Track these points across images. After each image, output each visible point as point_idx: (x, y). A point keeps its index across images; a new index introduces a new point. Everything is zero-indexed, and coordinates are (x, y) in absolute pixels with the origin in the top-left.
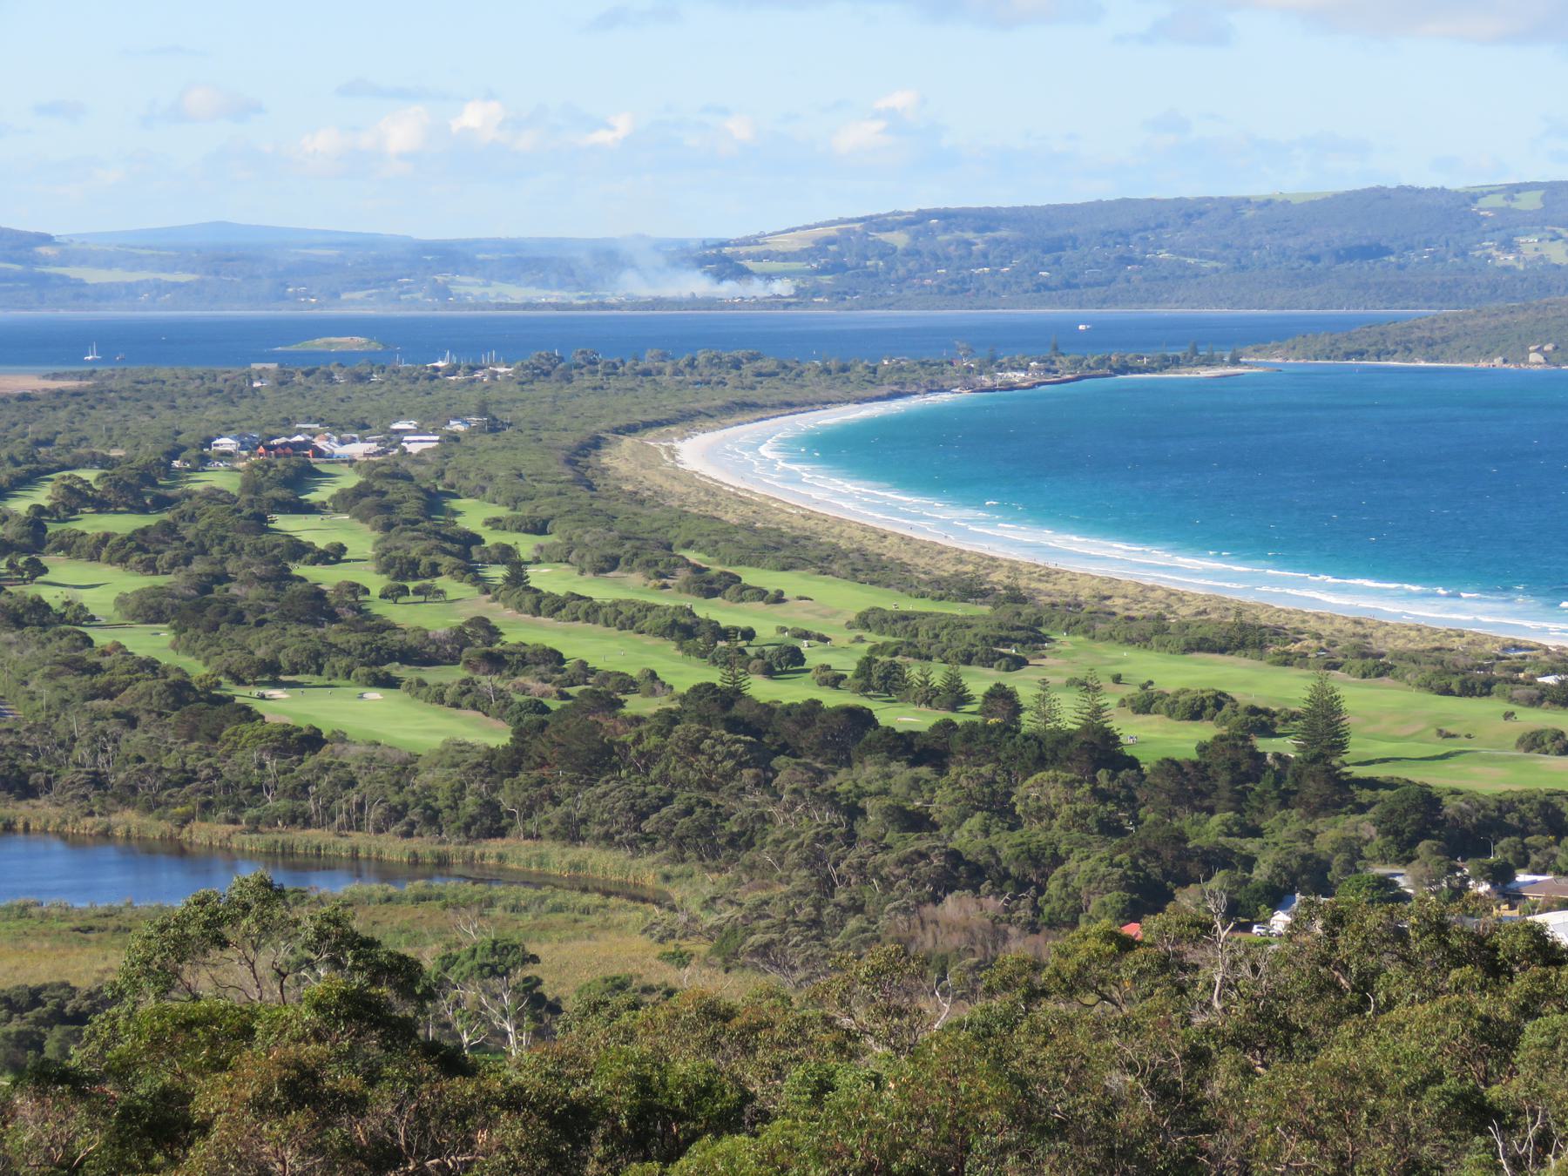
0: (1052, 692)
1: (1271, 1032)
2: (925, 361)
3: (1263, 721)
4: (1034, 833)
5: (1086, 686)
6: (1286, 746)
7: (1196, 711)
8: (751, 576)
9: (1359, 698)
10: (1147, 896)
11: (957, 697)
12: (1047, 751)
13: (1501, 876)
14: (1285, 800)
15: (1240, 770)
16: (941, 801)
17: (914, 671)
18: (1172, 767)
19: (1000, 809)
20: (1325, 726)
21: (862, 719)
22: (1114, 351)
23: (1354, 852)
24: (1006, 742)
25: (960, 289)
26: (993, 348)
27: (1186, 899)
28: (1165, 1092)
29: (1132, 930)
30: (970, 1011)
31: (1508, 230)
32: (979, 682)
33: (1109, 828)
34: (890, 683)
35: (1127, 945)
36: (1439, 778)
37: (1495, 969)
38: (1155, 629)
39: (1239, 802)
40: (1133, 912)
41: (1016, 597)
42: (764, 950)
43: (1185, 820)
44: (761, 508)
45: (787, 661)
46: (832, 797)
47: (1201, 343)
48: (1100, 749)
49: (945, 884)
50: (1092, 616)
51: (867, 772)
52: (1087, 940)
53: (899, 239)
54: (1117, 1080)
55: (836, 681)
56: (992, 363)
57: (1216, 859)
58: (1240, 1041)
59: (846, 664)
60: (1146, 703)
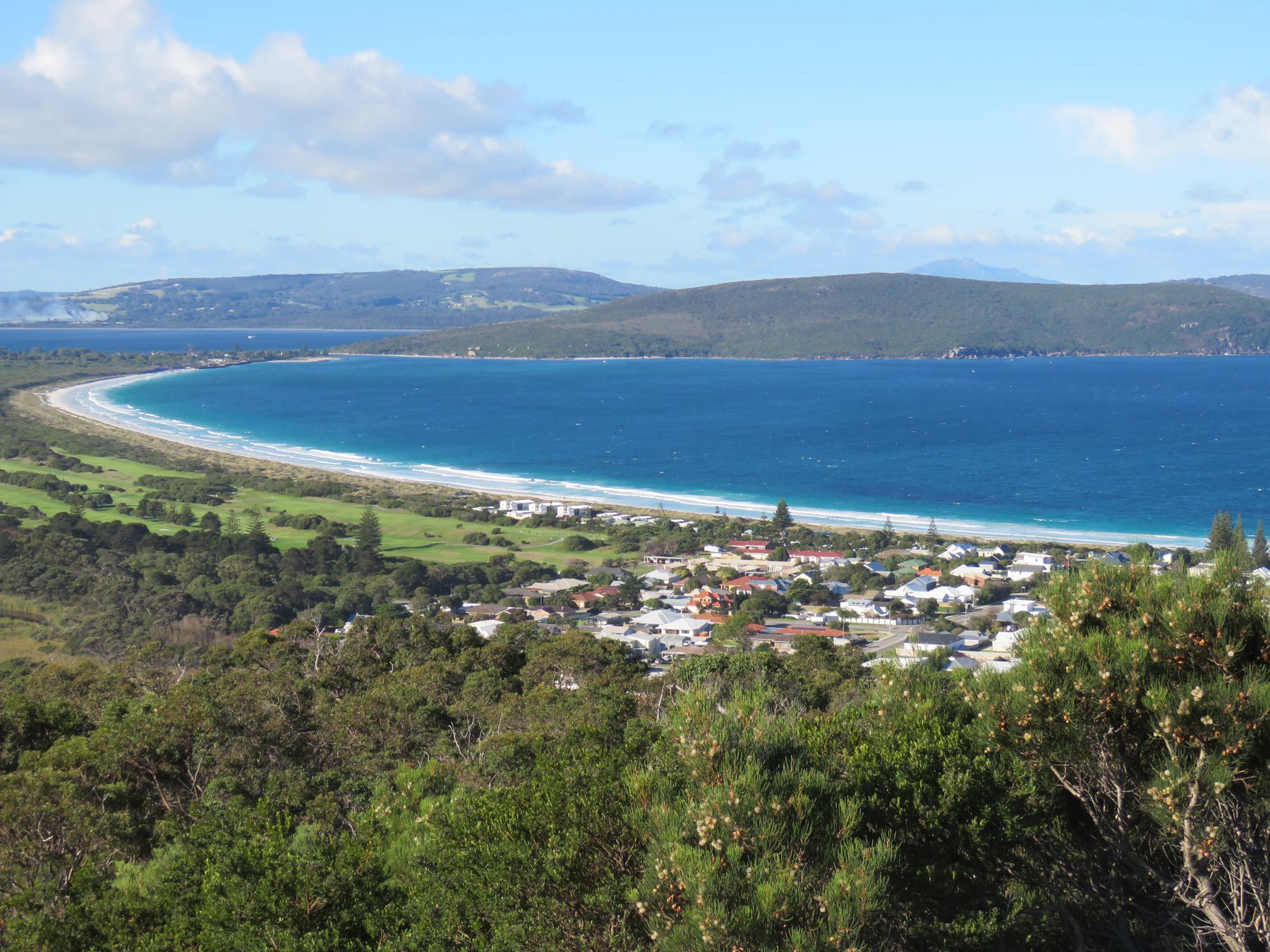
0: (236, 516)
1: (343, 681)
2: (172, 353)
3: (341, 529)
4: (228, 585)
6: (352, 542)
8: (86, 460)
9: (387, 518)
10: (283, 615)
11: (189, 519)
12: (234, 545)
13: (456, 604)
14: (351, 568)
15: (327, 554)
16: (181, 569)
17: (167, 506)
18: (295, 552)
20: (370, 531)
21: (142, 530)
22: (267, 348)
23: (384, 594)
24: (213, 541)
25: (190, 318)
26: (206, 347)
27: (303, 617)
28: (291, 711)
30: (193, 674)
32: (200, 511)
33: (265, 583)
34: (154, 511)
35: (272, 640)
36: (426, 557)
37: (453, 651)
38: (288, 484)
39: (328, 569)
40: (276, 623)
41: (218, 469)
42: (92, 645)
43: (301, 578)
45: (103, 501)
46: (126, 569)
48: (260, 544)
49: (183, 611)
50: (257, 479)
51: (144, 556)
53: (159, 293)
54: (267, 706)
55: (128, 511)
56: (206, 355)
57: (317, 597)
59: (134, 503)
60: (283, 521)
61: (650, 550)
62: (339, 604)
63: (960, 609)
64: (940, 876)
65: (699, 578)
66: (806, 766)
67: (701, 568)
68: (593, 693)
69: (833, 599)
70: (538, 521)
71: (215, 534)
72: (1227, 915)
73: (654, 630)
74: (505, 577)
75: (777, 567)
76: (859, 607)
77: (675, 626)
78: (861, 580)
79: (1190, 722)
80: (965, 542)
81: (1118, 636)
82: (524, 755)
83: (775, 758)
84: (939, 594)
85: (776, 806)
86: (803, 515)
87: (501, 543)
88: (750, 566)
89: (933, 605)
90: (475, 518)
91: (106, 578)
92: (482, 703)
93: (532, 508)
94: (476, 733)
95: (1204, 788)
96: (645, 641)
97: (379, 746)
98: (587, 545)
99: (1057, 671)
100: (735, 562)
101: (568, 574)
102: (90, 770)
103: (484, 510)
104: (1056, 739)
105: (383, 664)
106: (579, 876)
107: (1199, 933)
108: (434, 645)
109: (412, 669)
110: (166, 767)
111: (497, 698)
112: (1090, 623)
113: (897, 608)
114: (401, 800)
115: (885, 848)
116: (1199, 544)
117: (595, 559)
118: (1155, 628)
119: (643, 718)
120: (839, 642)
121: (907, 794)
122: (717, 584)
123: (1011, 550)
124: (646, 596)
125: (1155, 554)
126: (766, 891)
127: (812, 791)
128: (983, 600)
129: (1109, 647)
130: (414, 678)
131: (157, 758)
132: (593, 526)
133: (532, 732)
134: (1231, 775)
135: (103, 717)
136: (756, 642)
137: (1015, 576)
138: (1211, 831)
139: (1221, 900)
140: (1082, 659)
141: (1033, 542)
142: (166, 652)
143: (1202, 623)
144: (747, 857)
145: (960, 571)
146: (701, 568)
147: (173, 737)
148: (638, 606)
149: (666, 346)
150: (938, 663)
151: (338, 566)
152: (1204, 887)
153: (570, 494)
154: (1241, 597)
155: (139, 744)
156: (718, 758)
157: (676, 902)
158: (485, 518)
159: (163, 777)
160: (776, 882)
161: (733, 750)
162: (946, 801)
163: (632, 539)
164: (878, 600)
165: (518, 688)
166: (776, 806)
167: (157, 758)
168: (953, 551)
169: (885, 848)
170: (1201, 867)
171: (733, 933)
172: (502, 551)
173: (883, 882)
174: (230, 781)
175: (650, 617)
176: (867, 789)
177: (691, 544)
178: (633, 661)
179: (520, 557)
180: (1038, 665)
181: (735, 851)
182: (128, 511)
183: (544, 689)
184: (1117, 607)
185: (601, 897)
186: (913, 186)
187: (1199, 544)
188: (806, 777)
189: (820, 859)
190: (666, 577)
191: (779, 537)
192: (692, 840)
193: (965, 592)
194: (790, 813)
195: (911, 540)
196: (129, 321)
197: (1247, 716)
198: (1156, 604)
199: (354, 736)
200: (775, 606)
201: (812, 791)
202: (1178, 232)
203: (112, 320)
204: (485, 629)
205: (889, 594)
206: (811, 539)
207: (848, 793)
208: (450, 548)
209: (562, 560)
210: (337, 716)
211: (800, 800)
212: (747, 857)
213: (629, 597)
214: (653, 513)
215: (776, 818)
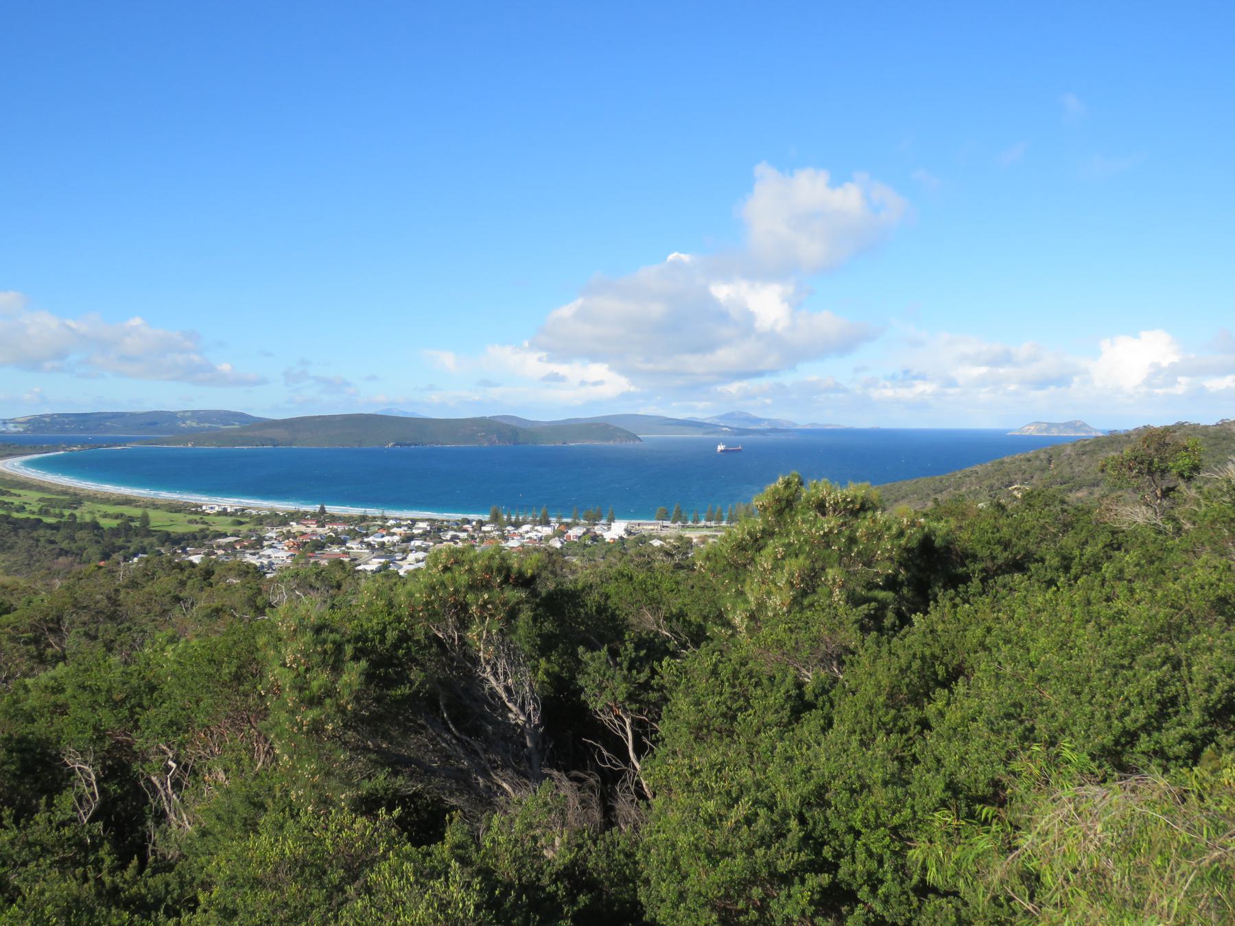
0: (84, 514)
1: (134, 584)
2: (54, 444)
3: (132, 519)
4: (80, 544)
5: (91, 512)
6: (137, 524)
7: (117, 517)
8: (13, 491)
9: (152, 514)
10: (106, 556)
11: (62, 516)
12: (83, 526)
13: (184, 549)
14: (137, 535)
15: (125, 528)
16: (58, 538)
17: (52, 510)
18: (112, 529)
19: (72, 539)
20: (145, 519)
21: (39, 521)
22: (97, 443)
23: (152, 546)
24: (73, 525)
25: (63, 430)
26: (70, 442)
27: (115, 556)
28: (109, 598)
29: (102, 563)
30: (65, 583)
31: (184, 419)
32: (67, 512)
33: (97, 542)
34: (46, 513)
35: (100, 568)
36: (170, 529)
37: (182, 570)
38: (108, 500)
39: (126, 536)
40: (103, 559)
41: (75, 494)
42: (16, 571)
43: (114, 540)
44: (15, 476)
45: (21, 509)
46: (32, 538)
47: (116, 442)
48: (95, 526)
49: (59, 555)
50: (94, 498)
51: (41, 532)
52: (92, 566)
53: (48, 420)
54: (99, 597)
55: (33, 513)
56: (69, 446)
57: (121, 548)
58: (126, 587)
59: (36, 509)
60: (105, 516)
61: (268, 524)
62: (131, 550)
63: (394, 545)
64: (386, 673)
65: (288, 535)
66: (332, 631)
67: (289, 531)
68: (243, 586)
69: (343, 543)
70: (219, 514)
71: (74, 522)
72: (497, 680)
73: (269, 557)
74: (205, 537)
75: (320, 530)
76: (354, 545)
77: (279, 555)
78: (354, 535)
79: (483, 607)
80: (396, 519)
81: (457, 574)
82: (217, 612)
83: (318, 630)
84: (386, 539)
85: (319, 649)
86: (332, 509)
87: (204, 523)
88: (309, 530)
89: (383, 544)
90: (192, 513)
91: (22, 541)
92: (195, 592)
93: (217, 508)
94: (192, 604)
95: (488, 632)
96: (265, 562)
97: (149, 611)
98: (241, 523)
99: (433, 588)
100: (303, 529)
101: (232, 535)
102: (15, 628)
103: (196, 510)
104: (433, 615)
105: (150, 576)
106: (238, 678)
107: (486, 687)
108: (174, 568)
109: (165, 579)
110: (51, 625)
111: (202, 589)
112: (446, 569)
113: (369, 545)
114: (157, 646)
115: (363, 664)
116: (486, 517)
117: (244, 529)
118: (470, 571)
119: (265, 595)
120: (347, 560)
121: (373, 640)
122: (295, 537)
123: (414, 521)
124: (265, 543)
125: (469, 522)
126: (315, 684)
127: (334, 642)
128: (403, 541)
129: (454, 579)
130: (165, 583)
131: (46, 621)
132: (242, 515)
133: (217, 603)
134: (500, 626)
135: (20, 604)
136: (312, 561)
137: (416, 532)
138: (491, 648)
139: (495, 674)
140: (443, 584)
141: (423, 517)
142: (51, 573)
143: (488, 569)
144: (307, 670)
145: (395, 530)
146: (289, 531)
147: (53, 614)
148: (262, 547)
149: (275, 443)
150: (385, 567)
151: (131, 533)
152: (488, 669)
153: (231, 503)
154: (503, 559)
155: (38, 616)
156: (295, 630)
157: (277, 690)
158: (196, 513)
159: (50, 630)
160: (319, 680)
161: (301, 627)
162: (388, 643)
163: (260, 520)
164: (362, 542)
165: (211, 585)
166: (319, 649)
167: (46, 621)
168: (391, 522)
169: (363, 664)
170: (488, 662)
171: (302, 702)
172: (204, 526)
173: (363, 678)
174: (82, 630)
175: (267, 552)
176: (357, 639)
177: (284, 521)
178: (259, 572)
179: (212, 528)
180: (425, 587)
181: (302, 669)
182: (33, 513)
183: (222, 585)
184: (456, 562)
185: (247, 687)
186: (373, 378)
187: (486, 517)
188: (332, 636)
189: (337, 669)
190: (274, 535)
191: (321, 518)
192: (284, 665)
193: (396, 538)
194: (325, 652)
195: (374, 518)
196: (34, 431)
197: (504, 604)
198: (471, 561)
199: (138, 608)
200: (320, 546)
201: (334, 642)
202: (477, 398)
203: (26, 431)
204: (196, 559)
205: (366, 540)
206: (334, 519)
207: (349, 641)
208: (181, 525)
209: (230, 530)
210: (129, 599)
211: (329, 646)
212: (307, 670)
213: (258, 544)
214: (269, 509)
215: (320, 654)
